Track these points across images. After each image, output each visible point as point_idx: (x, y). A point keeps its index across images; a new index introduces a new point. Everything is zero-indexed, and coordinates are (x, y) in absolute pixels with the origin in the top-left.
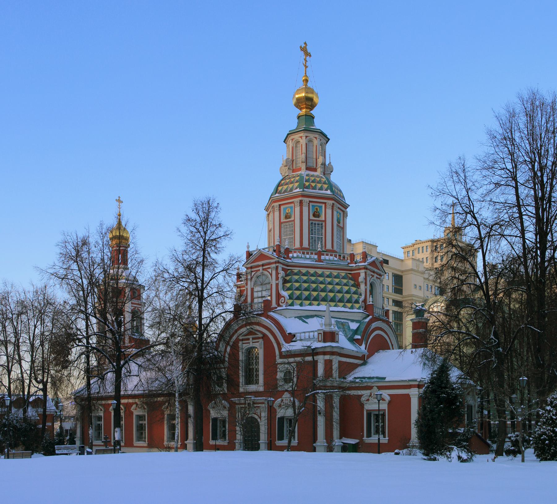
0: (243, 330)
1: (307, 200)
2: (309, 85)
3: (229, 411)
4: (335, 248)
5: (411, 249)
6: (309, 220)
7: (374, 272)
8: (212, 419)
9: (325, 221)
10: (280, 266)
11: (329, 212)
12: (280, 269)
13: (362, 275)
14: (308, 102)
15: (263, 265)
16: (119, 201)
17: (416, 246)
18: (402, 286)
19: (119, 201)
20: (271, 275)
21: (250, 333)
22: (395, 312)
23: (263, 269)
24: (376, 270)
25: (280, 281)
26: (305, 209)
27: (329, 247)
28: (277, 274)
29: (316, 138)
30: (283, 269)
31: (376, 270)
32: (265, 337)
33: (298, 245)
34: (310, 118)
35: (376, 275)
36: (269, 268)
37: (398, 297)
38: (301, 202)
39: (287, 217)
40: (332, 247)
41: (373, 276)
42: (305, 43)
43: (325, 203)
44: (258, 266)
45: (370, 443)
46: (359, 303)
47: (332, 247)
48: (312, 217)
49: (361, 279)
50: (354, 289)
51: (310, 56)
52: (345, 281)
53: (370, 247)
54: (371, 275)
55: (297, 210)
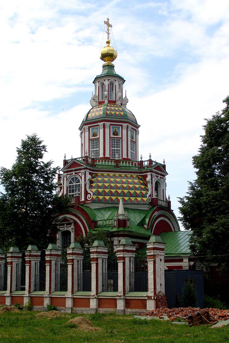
1: (107, 124)
2: (110, 44)
6: (110, 137)
7: (158, 174)
9: (122, 138)
11: (125, 131)
12: (87, 174)
14: (108, 57)
15: (75, 170)
20: (81, 177)
23: (75, 173)
24: (160, 172)
26: (107, 130)
29: (115, 80)
31: (160, 172)
33: (101, 156)
35: (160, 176)
36: (80, 173)
39: (94, 135)
40: (127, 156)
41: (157, 177)
42: (108, 19)
43: (122, 125)
44: (72, 171)
46: (146, 197)
47: (127, 156)
48: (112, 136)
51: (111, 26)
54: (156, 176)
55: (102, 131)
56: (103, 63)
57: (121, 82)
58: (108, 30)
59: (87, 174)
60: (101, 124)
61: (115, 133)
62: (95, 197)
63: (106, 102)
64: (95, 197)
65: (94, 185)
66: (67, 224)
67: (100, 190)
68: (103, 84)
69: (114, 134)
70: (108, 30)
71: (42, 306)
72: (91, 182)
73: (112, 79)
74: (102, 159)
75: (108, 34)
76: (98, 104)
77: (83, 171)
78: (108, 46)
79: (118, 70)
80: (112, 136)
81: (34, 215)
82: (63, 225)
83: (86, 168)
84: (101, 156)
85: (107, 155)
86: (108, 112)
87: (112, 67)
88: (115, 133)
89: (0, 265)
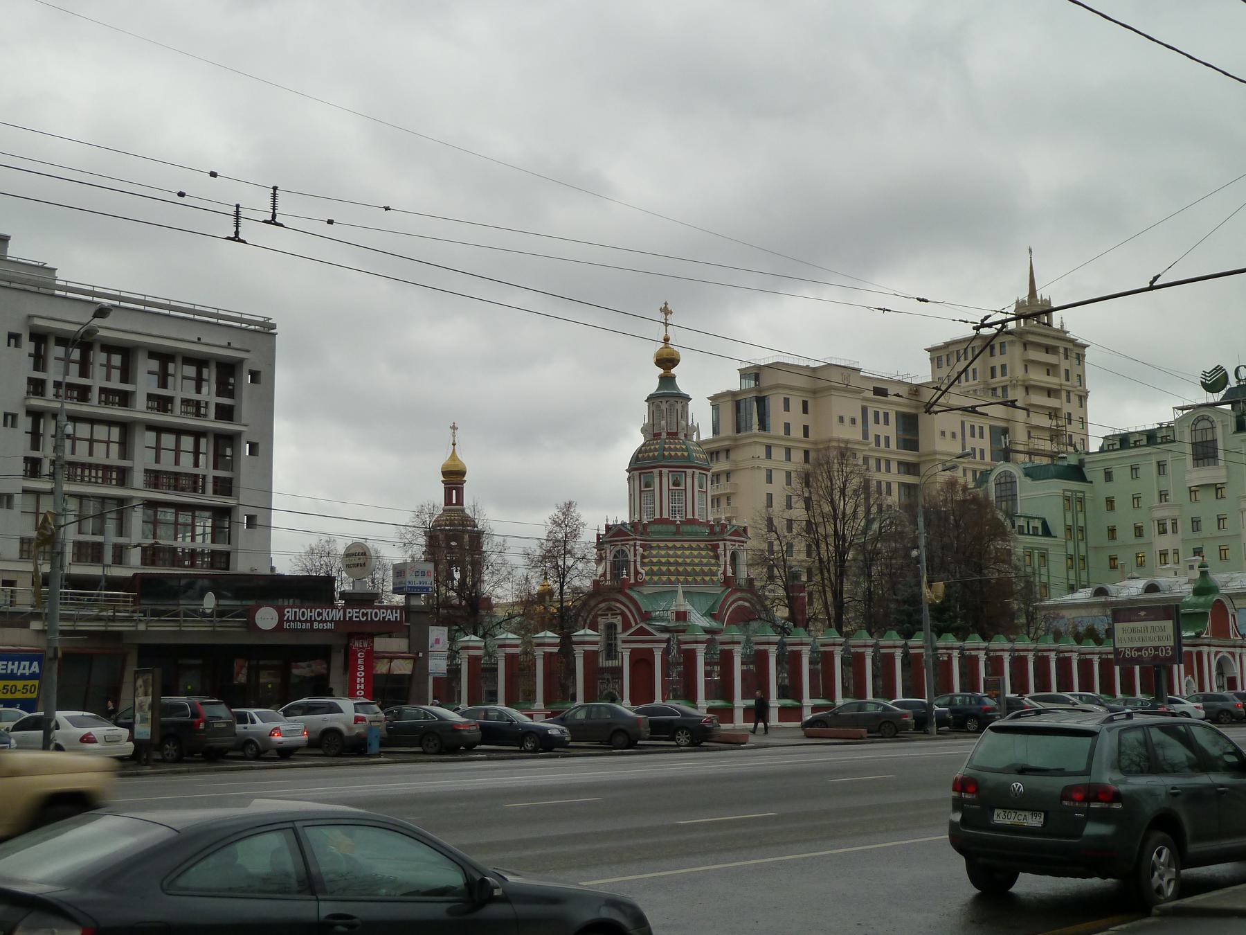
0: (601, 605)
3: (633, 525)
4: (696, 517)
5: (943, 353)
8: (434, 679)
10: (638, 543)
11: (689, 481)
13: (722, 547)
14: (667, 361)
16: (454, 428)
17: (952, 348)
18: (917, 434)
19: (454, 428)
21: (609, 609)
22: (901, 485)
25: (639, 559)
27: (690, 516)
30: (641, 546)
32: (623, 614)
34: (667, 380)
37: (908, 456)
38: (660, 473)
39: (647, 485)
45: (186, 645)
49: (721, 551)
50: (713, 561)
52: (704, 553)
53: (846, 372)
55: (657, 480)
56: (661, 371)
61: (676, 484)
62: (647, 578)
63: (664, 435)
72: (643, 557)
73: (672, 400)
79: (683, 385)
87: (674, 377)
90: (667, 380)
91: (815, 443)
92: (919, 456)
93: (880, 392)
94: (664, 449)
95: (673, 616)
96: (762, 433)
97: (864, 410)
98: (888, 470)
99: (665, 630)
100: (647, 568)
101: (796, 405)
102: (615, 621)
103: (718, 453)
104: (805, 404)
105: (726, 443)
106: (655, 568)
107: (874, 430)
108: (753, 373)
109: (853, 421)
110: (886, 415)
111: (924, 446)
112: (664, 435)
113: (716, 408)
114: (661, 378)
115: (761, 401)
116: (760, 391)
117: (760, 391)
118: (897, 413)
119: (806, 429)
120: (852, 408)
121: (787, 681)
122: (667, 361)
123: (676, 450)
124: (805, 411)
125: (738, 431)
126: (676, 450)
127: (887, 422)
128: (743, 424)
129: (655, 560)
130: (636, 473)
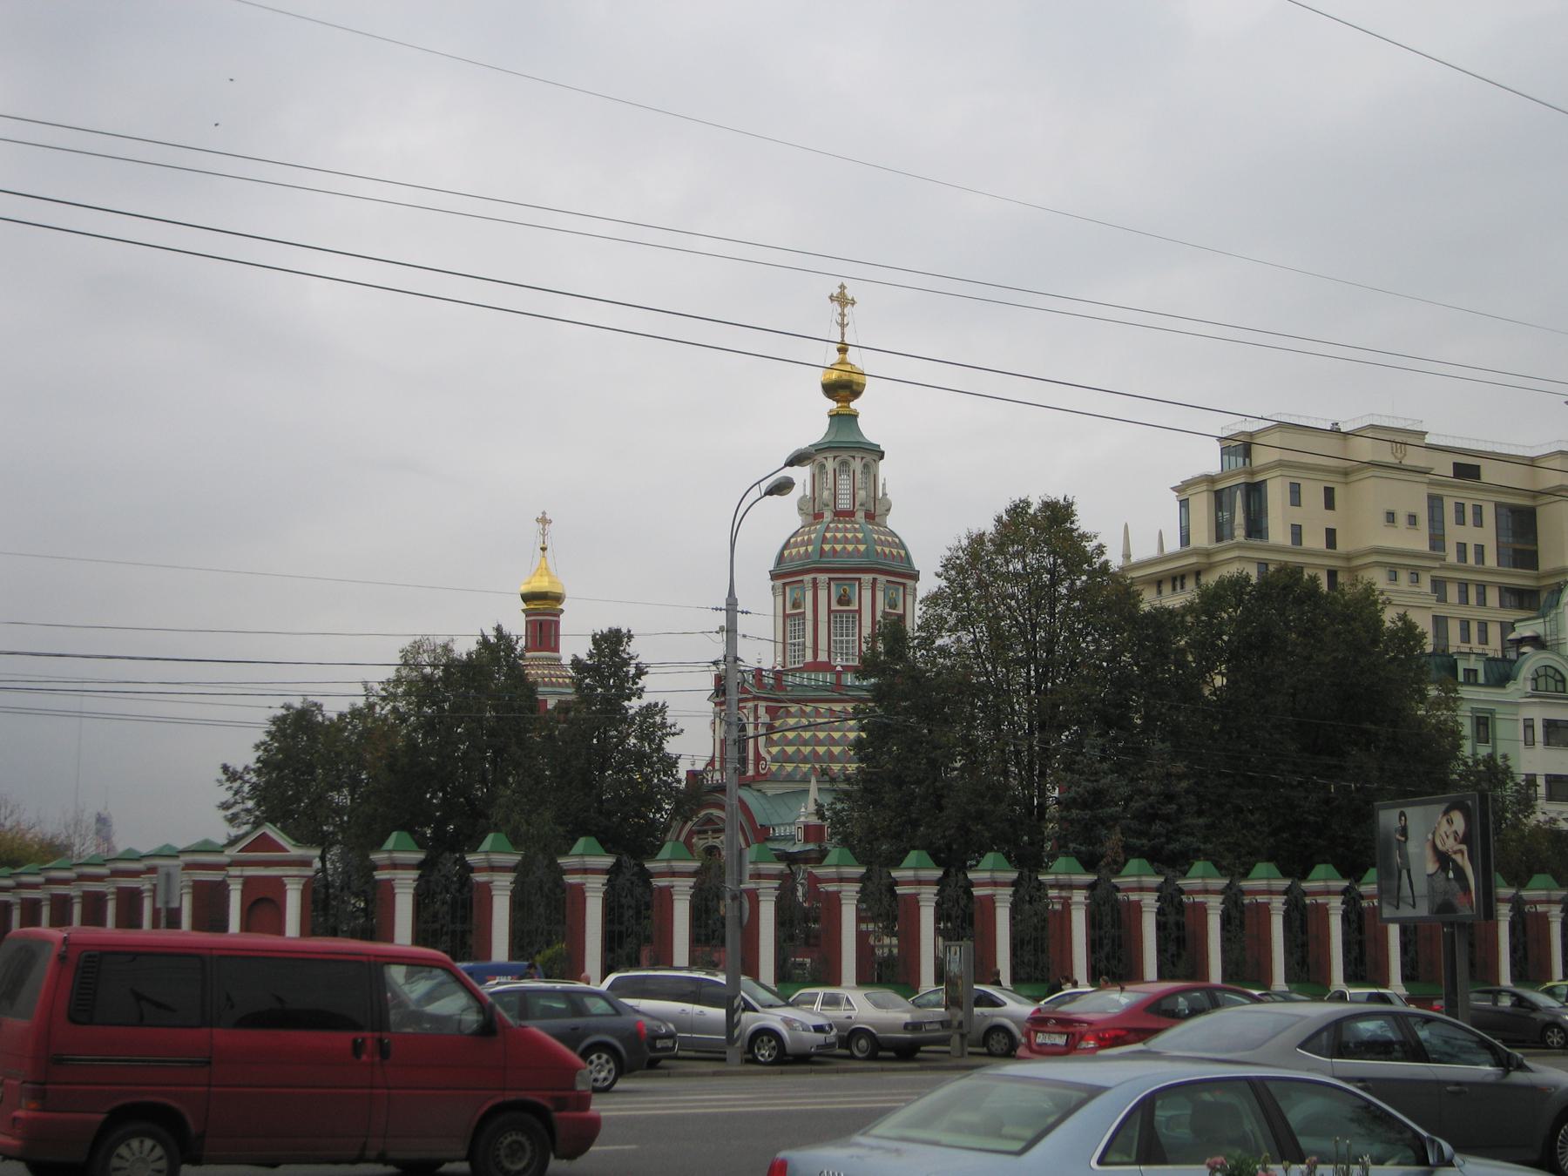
1: (823, 577)
6: (830, 611)
9: (859, 611)
11: (866, 594)
12: (762, 711)
14: (843, 389)
26: (822, 595)
28: (756, 718)
33: (809, 658)
34: (844, 420)
37: (1520, 579)
39: (796, 605)
48: (835, 607)
51: (853, 303)
55: (809, 595)
56: (832, 405)
57: (868, 458)
58: (843, 315)
59: (762, 711)
60: (808, 578)
61: (844, 600)
62: (774, 767)
63: (828, 516)
64: (774, 767)
65: (776, 736)
66: (714, 831)
67: (790, 750)
68: (823, 466)
69: (840, 602)
70: (843, 315)
71: (141, 900)
72: (771, 728)
73: (845, 455)
74: (808, 668)
75: (843, 326)
76: (810, 519)
77: (750, 704)
78: (843, 362)
79: (871, 428)
80: (835, 607)
81: (1219, 681)
82: (705, 832)
83: (759, 698)
84: (809, 658)
85: (823, 657)
86: (827, 547)
87: (854, 417)
88: (844, 600)
89: (7, 906)
90: (844, 420)
91: (1348, 557)
92: (1538, 578)
93: (1467, 472)
94: (824, 540)
95: (801, 835)
96: (1252, 542)
97: (1435, 503)
98: (1482, 601)
99: (784, 857)
100: (774, 750)
101: (1313, 494)
102: (717, 842)
103: (1183, 577)
104: (1329, 494)
105: (1193, 560)
106: (790, 750)
107: (1454, 534)
108: (1240, 447)
109: (1413, 519)
110: (1478, 510)
111: (1546, 563)
112: (828, 516)
113: (1184, 504)
114: (834, 417)
115: (1255, 492)
116: (1253, 473)
117: (1253, 473)
118: (1498, 505)
119: (1331, 535)
120: (1413, 498)
121: (895, 951)
122: (843, 389)
123: (846, 541)
124: (1330, 503)
125: (1219, 539)
126: (846, 541)
127: (1479, 522)
128: (1226, 531)
129: (791, 735)
130: (779, 583)
